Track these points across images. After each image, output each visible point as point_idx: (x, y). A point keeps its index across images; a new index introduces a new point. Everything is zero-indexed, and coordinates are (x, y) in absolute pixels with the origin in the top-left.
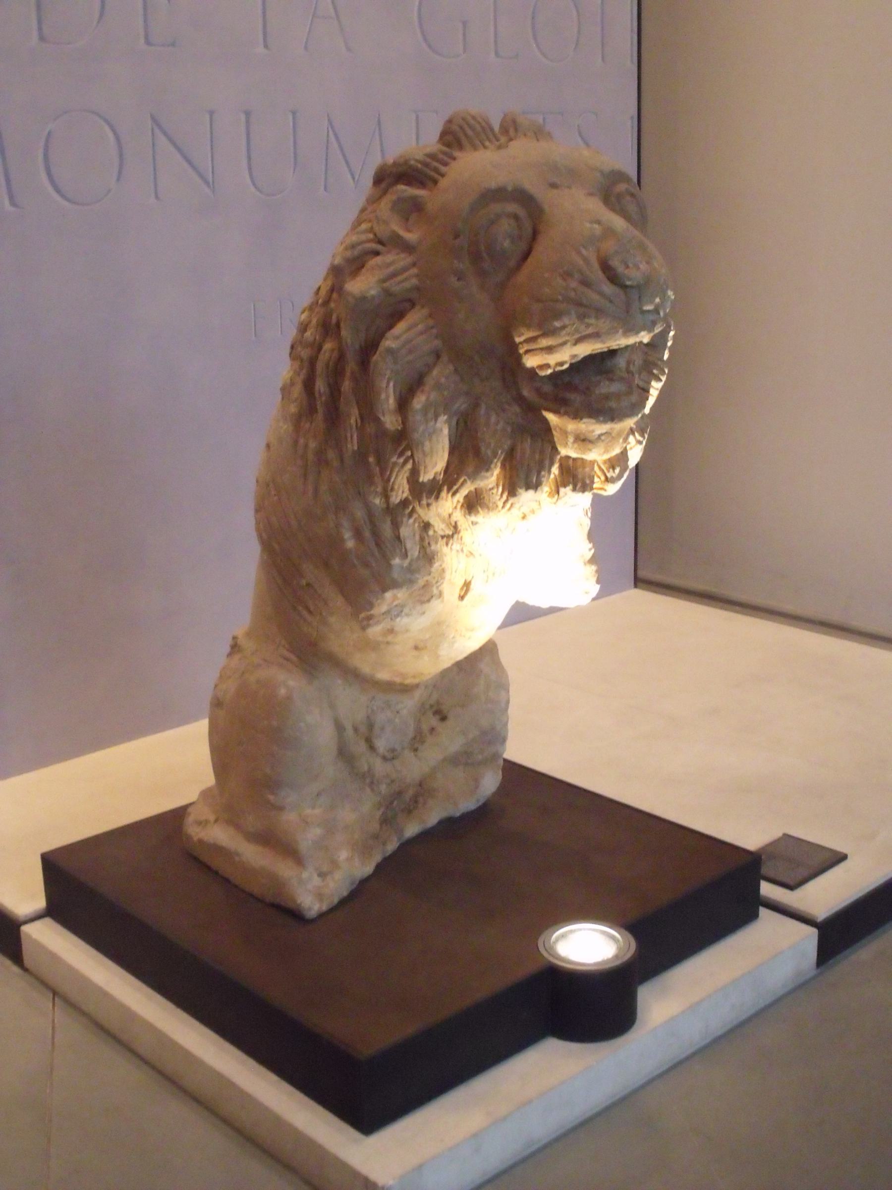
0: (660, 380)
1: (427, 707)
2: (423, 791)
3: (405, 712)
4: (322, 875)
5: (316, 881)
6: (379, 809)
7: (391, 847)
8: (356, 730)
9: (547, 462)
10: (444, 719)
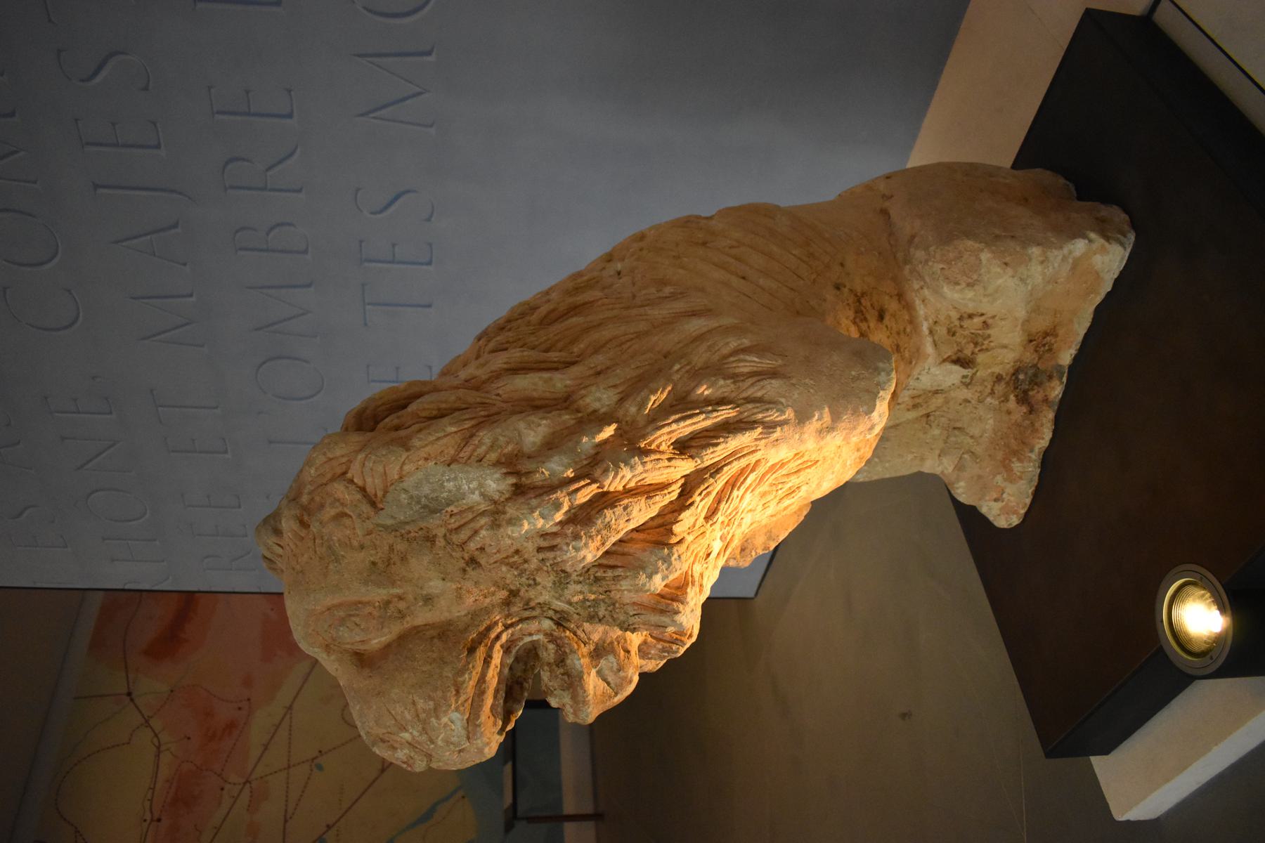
2: (1041, 341)
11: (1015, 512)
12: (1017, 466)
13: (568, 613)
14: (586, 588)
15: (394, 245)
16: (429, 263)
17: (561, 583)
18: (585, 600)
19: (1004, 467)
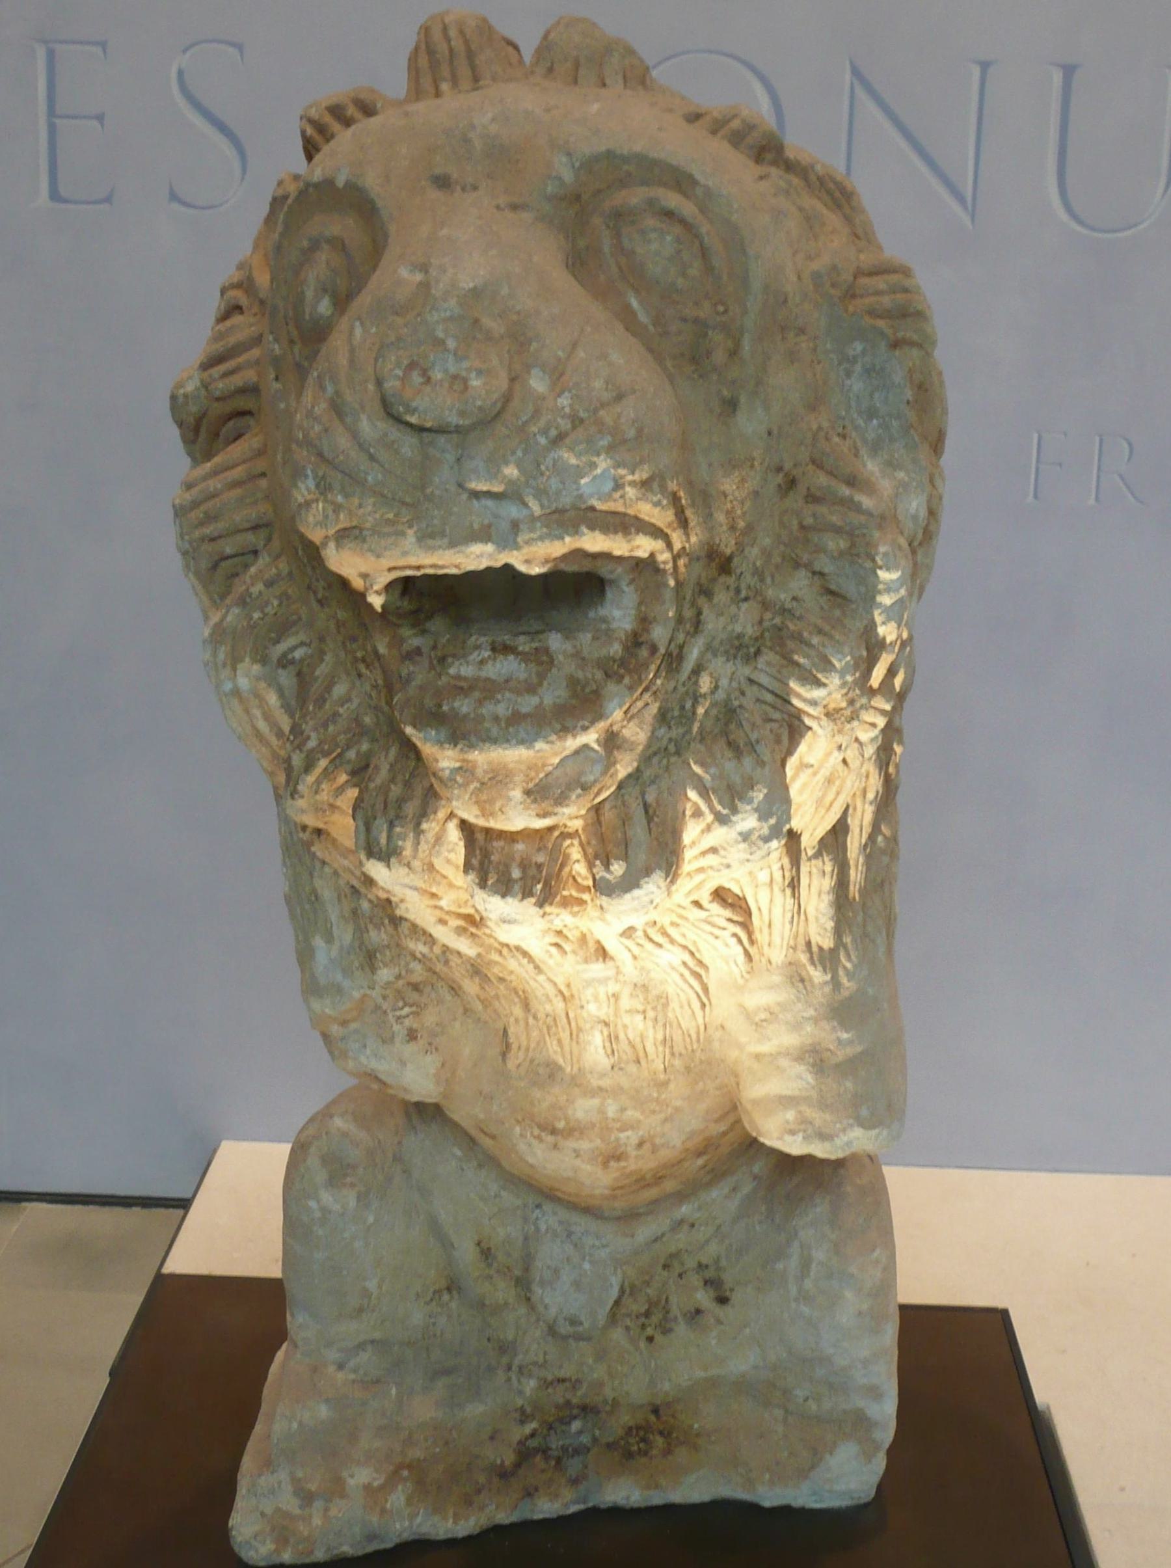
0: (819, 684)
1: (691, 1263)
2: (656, 1431)
3: (603, 1254)
4: (307, 1498)
5: (289, 1502)
6: (522, 1422)
7: (546, 1508)
8: (486, 1254)
9: (410, 808)
10: (722, 1300)
11: (282, 1540)
12: (397, 1499)
13: (678, 671)
14: (720, 695)
15: (100, 118)
16: (55, 195)
17: (738, 648)
18: (696, 698)
19: (396, 1472)
